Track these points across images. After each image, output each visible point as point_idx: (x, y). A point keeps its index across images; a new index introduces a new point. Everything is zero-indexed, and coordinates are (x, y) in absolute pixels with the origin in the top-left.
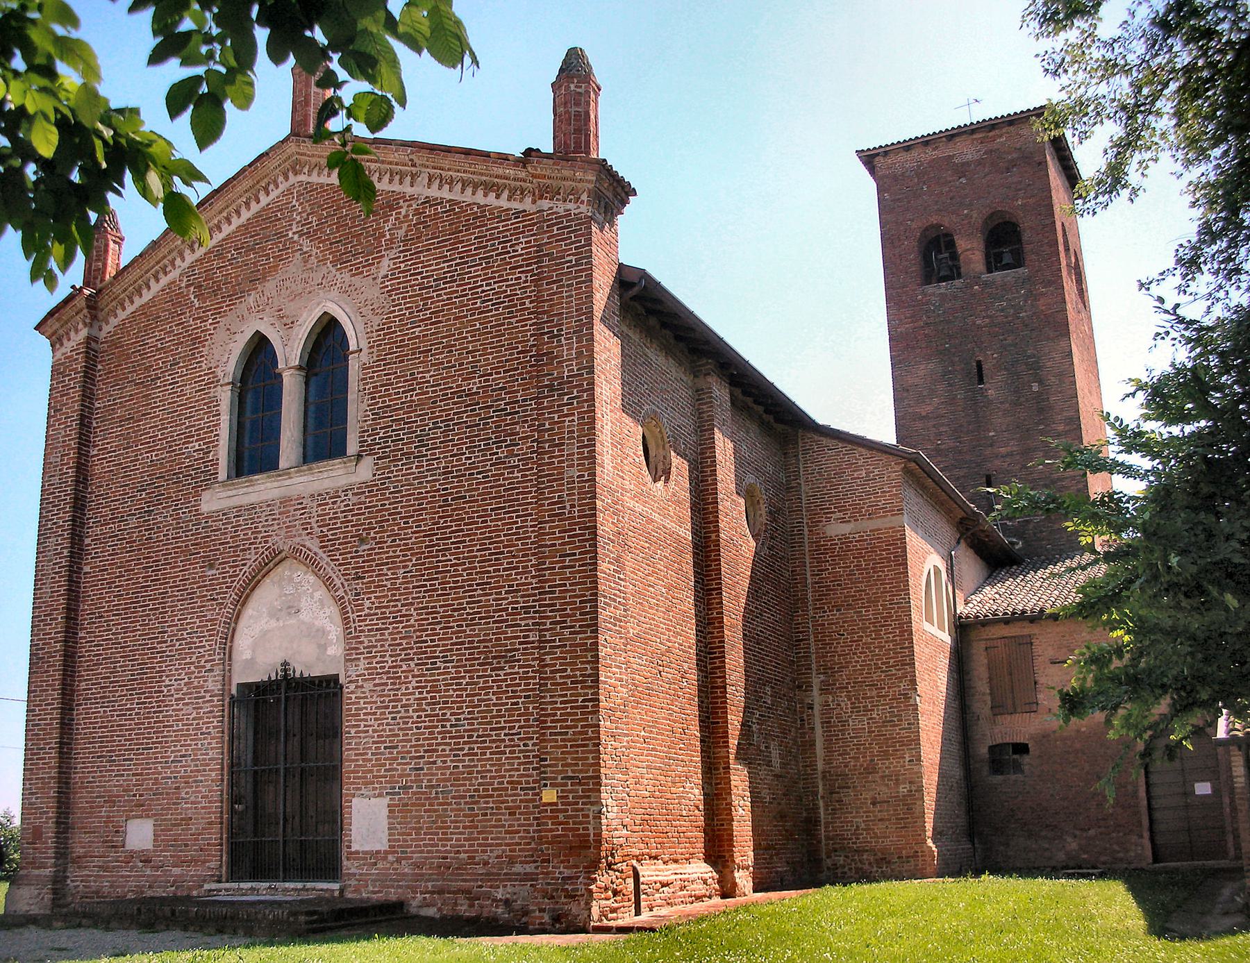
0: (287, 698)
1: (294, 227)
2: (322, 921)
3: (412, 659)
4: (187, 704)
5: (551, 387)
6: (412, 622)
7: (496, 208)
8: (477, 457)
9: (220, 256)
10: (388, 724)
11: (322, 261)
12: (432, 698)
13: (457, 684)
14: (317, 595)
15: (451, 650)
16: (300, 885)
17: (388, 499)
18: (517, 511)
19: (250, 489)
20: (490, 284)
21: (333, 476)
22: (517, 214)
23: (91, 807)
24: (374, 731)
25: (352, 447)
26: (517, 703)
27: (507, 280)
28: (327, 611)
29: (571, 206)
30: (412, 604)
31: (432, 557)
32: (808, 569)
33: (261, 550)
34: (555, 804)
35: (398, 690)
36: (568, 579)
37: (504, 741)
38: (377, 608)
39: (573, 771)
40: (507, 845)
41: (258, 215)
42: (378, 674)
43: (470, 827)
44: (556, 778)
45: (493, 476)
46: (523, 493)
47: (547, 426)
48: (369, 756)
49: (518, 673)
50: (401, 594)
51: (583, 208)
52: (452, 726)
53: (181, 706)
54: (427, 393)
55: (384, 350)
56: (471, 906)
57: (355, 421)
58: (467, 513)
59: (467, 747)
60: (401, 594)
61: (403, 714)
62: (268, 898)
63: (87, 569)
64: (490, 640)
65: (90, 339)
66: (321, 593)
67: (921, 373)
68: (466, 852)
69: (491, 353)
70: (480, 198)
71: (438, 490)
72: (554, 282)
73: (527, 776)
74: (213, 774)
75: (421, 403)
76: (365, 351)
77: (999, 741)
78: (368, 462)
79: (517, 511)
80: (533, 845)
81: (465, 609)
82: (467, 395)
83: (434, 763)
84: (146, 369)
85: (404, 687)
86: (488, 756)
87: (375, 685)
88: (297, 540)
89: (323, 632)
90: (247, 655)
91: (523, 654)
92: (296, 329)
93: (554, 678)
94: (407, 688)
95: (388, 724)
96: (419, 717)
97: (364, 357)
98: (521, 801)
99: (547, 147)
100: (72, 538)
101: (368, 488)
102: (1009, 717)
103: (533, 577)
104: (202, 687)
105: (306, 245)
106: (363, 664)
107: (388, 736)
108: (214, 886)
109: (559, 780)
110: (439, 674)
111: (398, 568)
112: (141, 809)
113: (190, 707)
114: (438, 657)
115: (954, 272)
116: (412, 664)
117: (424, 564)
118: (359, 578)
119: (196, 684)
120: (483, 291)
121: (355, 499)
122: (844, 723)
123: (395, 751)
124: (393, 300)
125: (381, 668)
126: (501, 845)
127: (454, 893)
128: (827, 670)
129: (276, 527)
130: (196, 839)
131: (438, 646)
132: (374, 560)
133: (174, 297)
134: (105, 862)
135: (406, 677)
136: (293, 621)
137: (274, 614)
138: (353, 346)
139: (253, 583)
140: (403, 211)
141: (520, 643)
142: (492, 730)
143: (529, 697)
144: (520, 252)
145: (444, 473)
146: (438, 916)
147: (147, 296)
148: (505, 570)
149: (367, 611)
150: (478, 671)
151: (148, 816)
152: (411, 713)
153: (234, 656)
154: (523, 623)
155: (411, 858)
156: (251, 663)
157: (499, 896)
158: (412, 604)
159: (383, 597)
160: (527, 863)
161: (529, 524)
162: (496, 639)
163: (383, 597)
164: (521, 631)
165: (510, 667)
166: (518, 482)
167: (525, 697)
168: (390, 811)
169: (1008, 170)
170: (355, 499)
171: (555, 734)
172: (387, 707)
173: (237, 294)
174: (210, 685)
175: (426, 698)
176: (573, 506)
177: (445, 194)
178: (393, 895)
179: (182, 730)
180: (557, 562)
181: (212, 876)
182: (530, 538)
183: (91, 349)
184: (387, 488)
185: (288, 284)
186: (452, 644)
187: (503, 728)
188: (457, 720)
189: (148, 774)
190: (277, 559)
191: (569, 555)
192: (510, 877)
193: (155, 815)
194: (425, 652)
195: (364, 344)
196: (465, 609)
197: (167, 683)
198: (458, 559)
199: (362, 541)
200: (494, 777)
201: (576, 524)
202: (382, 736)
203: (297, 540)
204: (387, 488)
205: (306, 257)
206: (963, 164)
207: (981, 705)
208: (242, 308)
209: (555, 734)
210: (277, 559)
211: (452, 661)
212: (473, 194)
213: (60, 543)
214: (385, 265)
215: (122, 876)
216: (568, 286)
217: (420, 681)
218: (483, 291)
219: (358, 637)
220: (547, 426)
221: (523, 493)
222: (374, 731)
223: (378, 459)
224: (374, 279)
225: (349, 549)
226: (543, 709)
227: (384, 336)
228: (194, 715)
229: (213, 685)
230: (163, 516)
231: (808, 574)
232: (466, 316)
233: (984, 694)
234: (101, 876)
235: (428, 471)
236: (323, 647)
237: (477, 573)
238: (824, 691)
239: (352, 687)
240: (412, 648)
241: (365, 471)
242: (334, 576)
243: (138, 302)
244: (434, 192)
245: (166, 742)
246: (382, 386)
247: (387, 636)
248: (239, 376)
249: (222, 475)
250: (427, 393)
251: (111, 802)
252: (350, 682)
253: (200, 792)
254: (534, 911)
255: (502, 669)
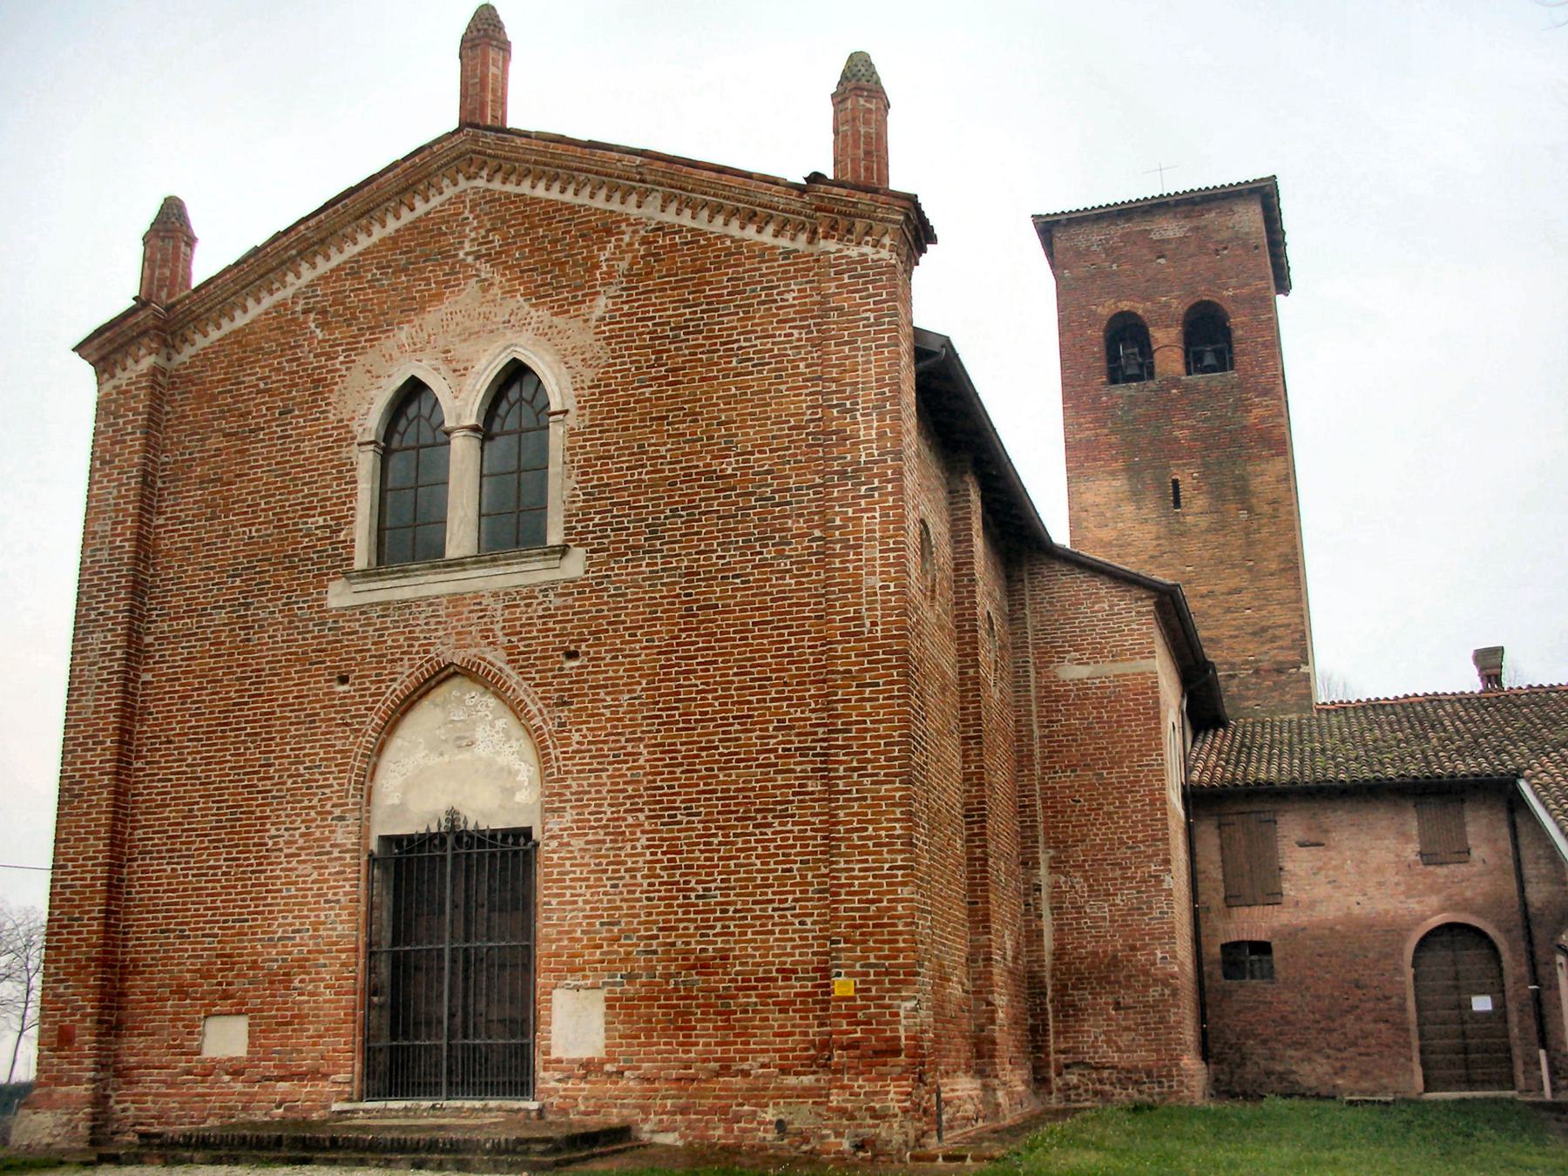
0: (456, 857)
1: (467, 247)
2: (557, 1150)
3: (641, 810)
4: (304, 862)
5: (842, 474)
6: (641, 762)
7: (756, 244)
8: (733, 556)
9: (355, 274)
10: (605, 893)
11: (512, 292)
12: (669, 860)
13: (705, 844)
14: (500, 724)
15: (698, 800)
16: (478, 1104)
17: (607, 603)
18: (791, 627)
19: (404, 582)
20: (749, 340)
21: (529, 573)
22: (787, 254)
23: (150, 1000)
24: (586, 902)
25: (555, 537)
26: (790, 870)
27: (773, 336)
28: (513, 742)
29: (867, 249)
30: (641, 739)
31: (671, 680)
32: (1034, 718)
33: (419, 663)
34: (853, 999)
35: (620, 849)
36: (869, 714)
37: (772, 917)
38: (590, 743)
39: (877, 957)
40: (775, 1051)
41: (413, 226)
42: (591, 828)
43: (724, 1028)
44: (853, 966)
45: (756, 581)
46: (797, 605)
47: (838, 522)
48: (578, 934)
49: (791, 831)
50: (624, 727)
51: (884, 254)
52: (698, 897)
53: (294, 864)
54: (663, 471)
55: (601, 413)
56: (729, 1130)
57: (559, 502)
58: (719, 626)
59: (719, 924)
60: (624, 727)
61: (627, 880)
62: (432, 1121)
63: (147, 677)
64: (753, 789)
65: (155, 371)
66: (506, 721)
67: (1103, 490)
68: (716, 1060)
69: (753, 427)
70: (734, 229)
71: (678, 596)
72: (846, 343)
73: (804, 963)
74: (344, 956)
75: (653, 485)
76: (574, 411)
77: (1234, 938)
78: (578, 556)
79: (791, 627)
80: (812, 1052)
81: (716, 748)
82: (718, 478)
83: (673, 944)
84: (241, 415)
85: (629, 845)
86: (750, 936)
87: (588, 842)
88: (474, 651)
89: (512, 773)
90: (394, 799)
91: (798, 808)
92: (469, 380)
93: (849, 839)
94: (634, 848)
95: (605, 893)
96: (650, 885)
97: (572, 420)
98: (797, 995)
99: (830, 176)
100: (129, 635)
101: (572, 587)
102: (1247, 910)
103: (812, 711)
104: (328, 839)
105: (485, 270)
106: (570, 815)
107: (605, 909)
108: (347, 1106)
109: (858, 968)
110: (679, 831)
111: (621, 692)
112: (229, 1002)
113: (309, 866)
114: (678, 808)
115: (1146, 371)
116: (641, 816)
117: (659, 688)
118: (565, 703)
119: (318, 835)
120: (740, 348)
121: (559, 602)
122: (1079, 909)
123: (616, 929)
124: (613, 351)
125: (596, 820)
126: (767, 1051)
127: (704, 1113)
128: (1057, 843)
129: (441, 633)
130: (314, 1044)
131: (679, 794)
132: (586, 681)
133: (284, 322)
134: (171, 1075)
135: (633, 833)
136: (465, 756)
137: (436, 748)
138: (555, 406)
139: (408, 704)
140: (626, 238)
141: (794, 794)
142: (754, 903)
143: (807, 862)
144: (791, 301)
145: (686, 575)
146: (680, 1143)
147: (241, 320)
148: (773, 700)
149: (576, 747)
150: (735, 827)
151: (239, 1013)
152: (639, 880)
153: (374, 799)
154: (798, 768)
155: (639, 1068)
156: (400, 810)
157: (768, 1117)
158: (641, 739)
159: (600, 729)
160: (804, 1074)
161: (806, 643)
162: (761, 788)
163: (600, 729)
164: (797, 778)
165: (781, 824)
166: (791, 591)
167: (802, 862)
168: (609, 1007)
169: (1217, 252)
170: (559, 602)
171: (852, 909)
172: (606, 871)
173: (380, 327)
174: (339, 837)
175: (660, 861)
176: (874, 624)
177: (686, 220)
178: (614, 1118)
179: (296, 897)
180: (854, 694)
181: (339, 1093)
182: (807, 661)
183: (160, 387)
184: (605, 590)
185: (458, 318)
186: (698, 793)
187: (772, 901)
188: (705, 889)
189: (241, 955)
190: (442, 676)
191: (869, 685)
192: (783, 1093)
193: (252, 1011)
194: (661, 802)
195: (571, 404)
196: (716, 748)
197: (273, 832)
198: (707, 684)
199: (572, 655)
200: (759, 965)
201: (880, 646)
202: (597, 909)
203: (474, 651)
204: (605, 590)
205: (486, 285)
206: (1163, 241)
207: (1214, 895)
208: (388, 345)
209: (852, 909)
210: (442, 676)
211: (699, 814)
212: (726, 224)
213: (107, 639)
214: (601, 305)
215: (198, 1095)
216: (865, 349)
217: (653, 839)
218: (740, 348)
219: (563, 780)
220: (838, 522)
221: (797, 605)
222: (586, 902)
223: (593, 551)
224: (586, 321)
225: (547, 670)
226: (834, 878)
227: (602, 397)
228: (315, 876)
229: (344, 836)
230: (268, 610)
231: (1035, 727)
232: (716, 378)
233: (1215, 880)
234: (167, 1095)
235: (663, 570)
236: (510, 792)
237: (733, 704)
238: (1055, 867)
239: (554, 844)
240: (641, 796)
241: (575, 565)
242: (528, 700)
243: (227, 327)
244: (670, 217)
245: (271, 912)
246: (597, 459)
247: (605, 780)
248: (382, 433)
249: (361, 559)
250: (663, 471)
251: (181, 992)
252: (552, 837)
253: (323, 980)
254: (828, 1136)
255: (769, 825)
